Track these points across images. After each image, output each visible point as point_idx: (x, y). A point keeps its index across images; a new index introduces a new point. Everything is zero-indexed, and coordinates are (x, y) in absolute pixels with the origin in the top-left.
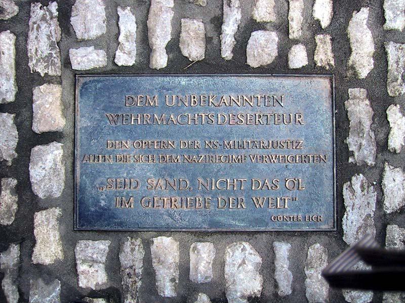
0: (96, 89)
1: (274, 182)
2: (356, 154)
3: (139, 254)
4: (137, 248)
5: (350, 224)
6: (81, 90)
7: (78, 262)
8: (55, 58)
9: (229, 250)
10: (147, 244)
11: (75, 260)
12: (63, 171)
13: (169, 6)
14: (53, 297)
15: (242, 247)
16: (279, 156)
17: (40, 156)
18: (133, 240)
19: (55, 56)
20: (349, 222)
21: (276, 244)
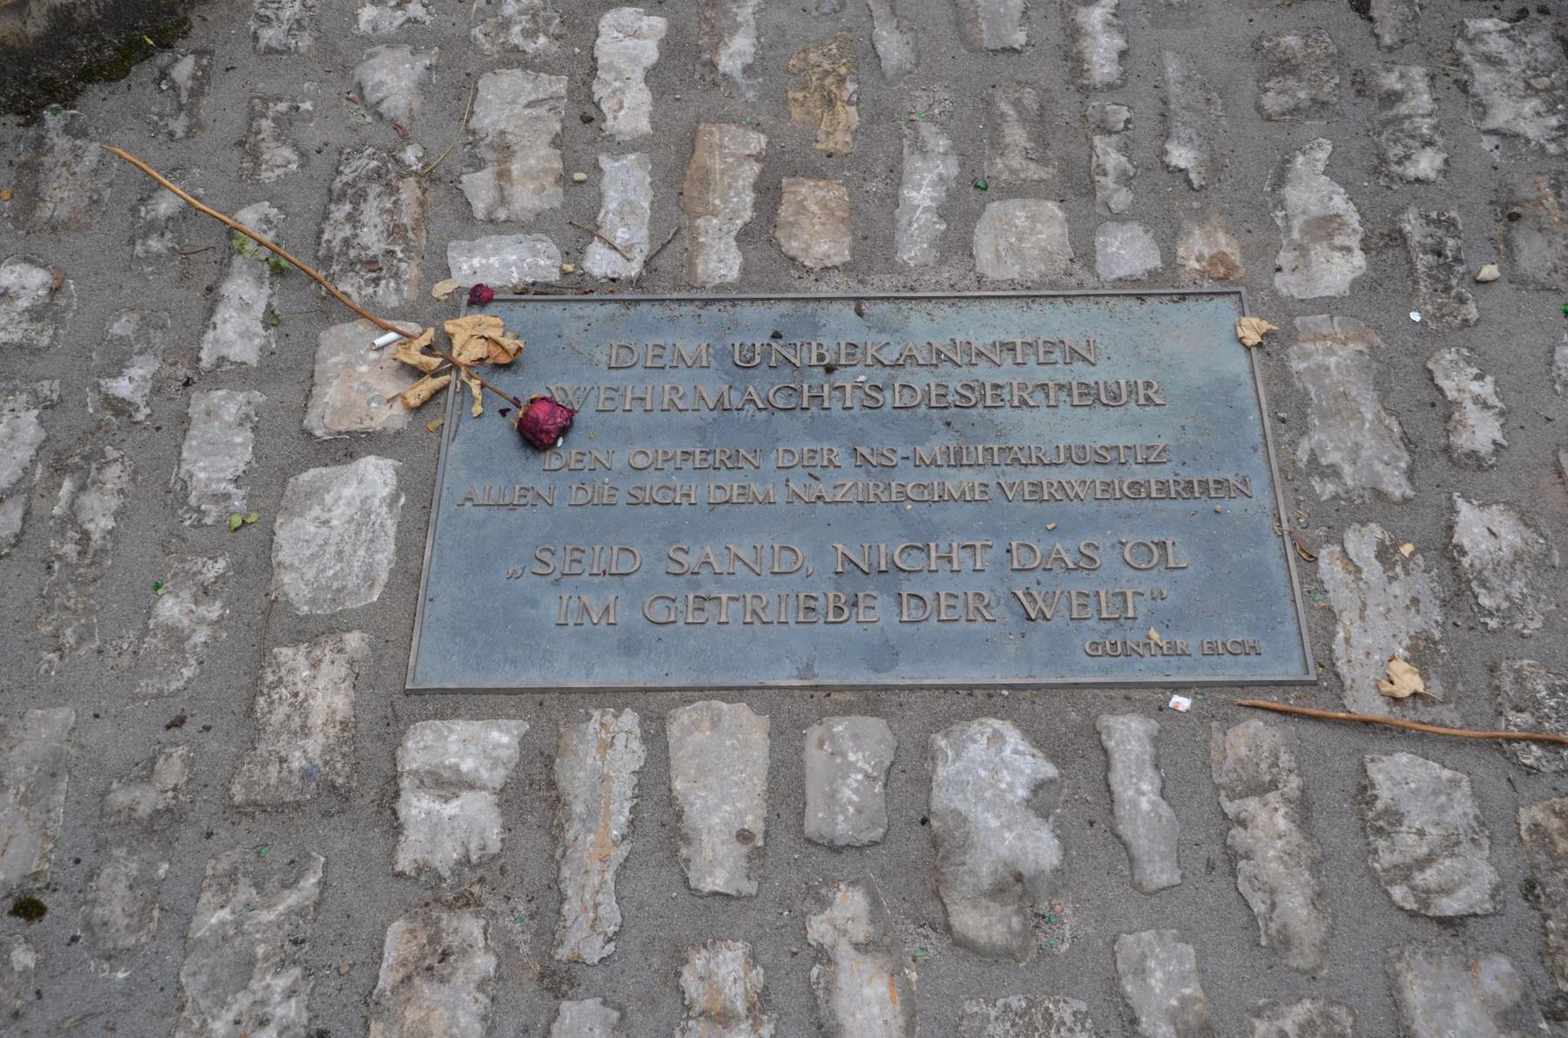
0: (1332, 1003)
1: (1128, 557)
2: (1347, 469)
3: (628, 756)
4: (620, 741)
5: (1362, 657)
6: (1225, 758)
7: (405, 783)
8: (400, 260)
9: (943, 743)
10: (655, 738)
11: (394, 778)
12: (392, 530)
13: (748, 152)
14: (290, 911)
15: (989, 730)
16: (1093, 482)
17: (314, 493)
18: (609, 718)
19: (400, 255)
20: (1358, 654)
21: (1107, 720)
